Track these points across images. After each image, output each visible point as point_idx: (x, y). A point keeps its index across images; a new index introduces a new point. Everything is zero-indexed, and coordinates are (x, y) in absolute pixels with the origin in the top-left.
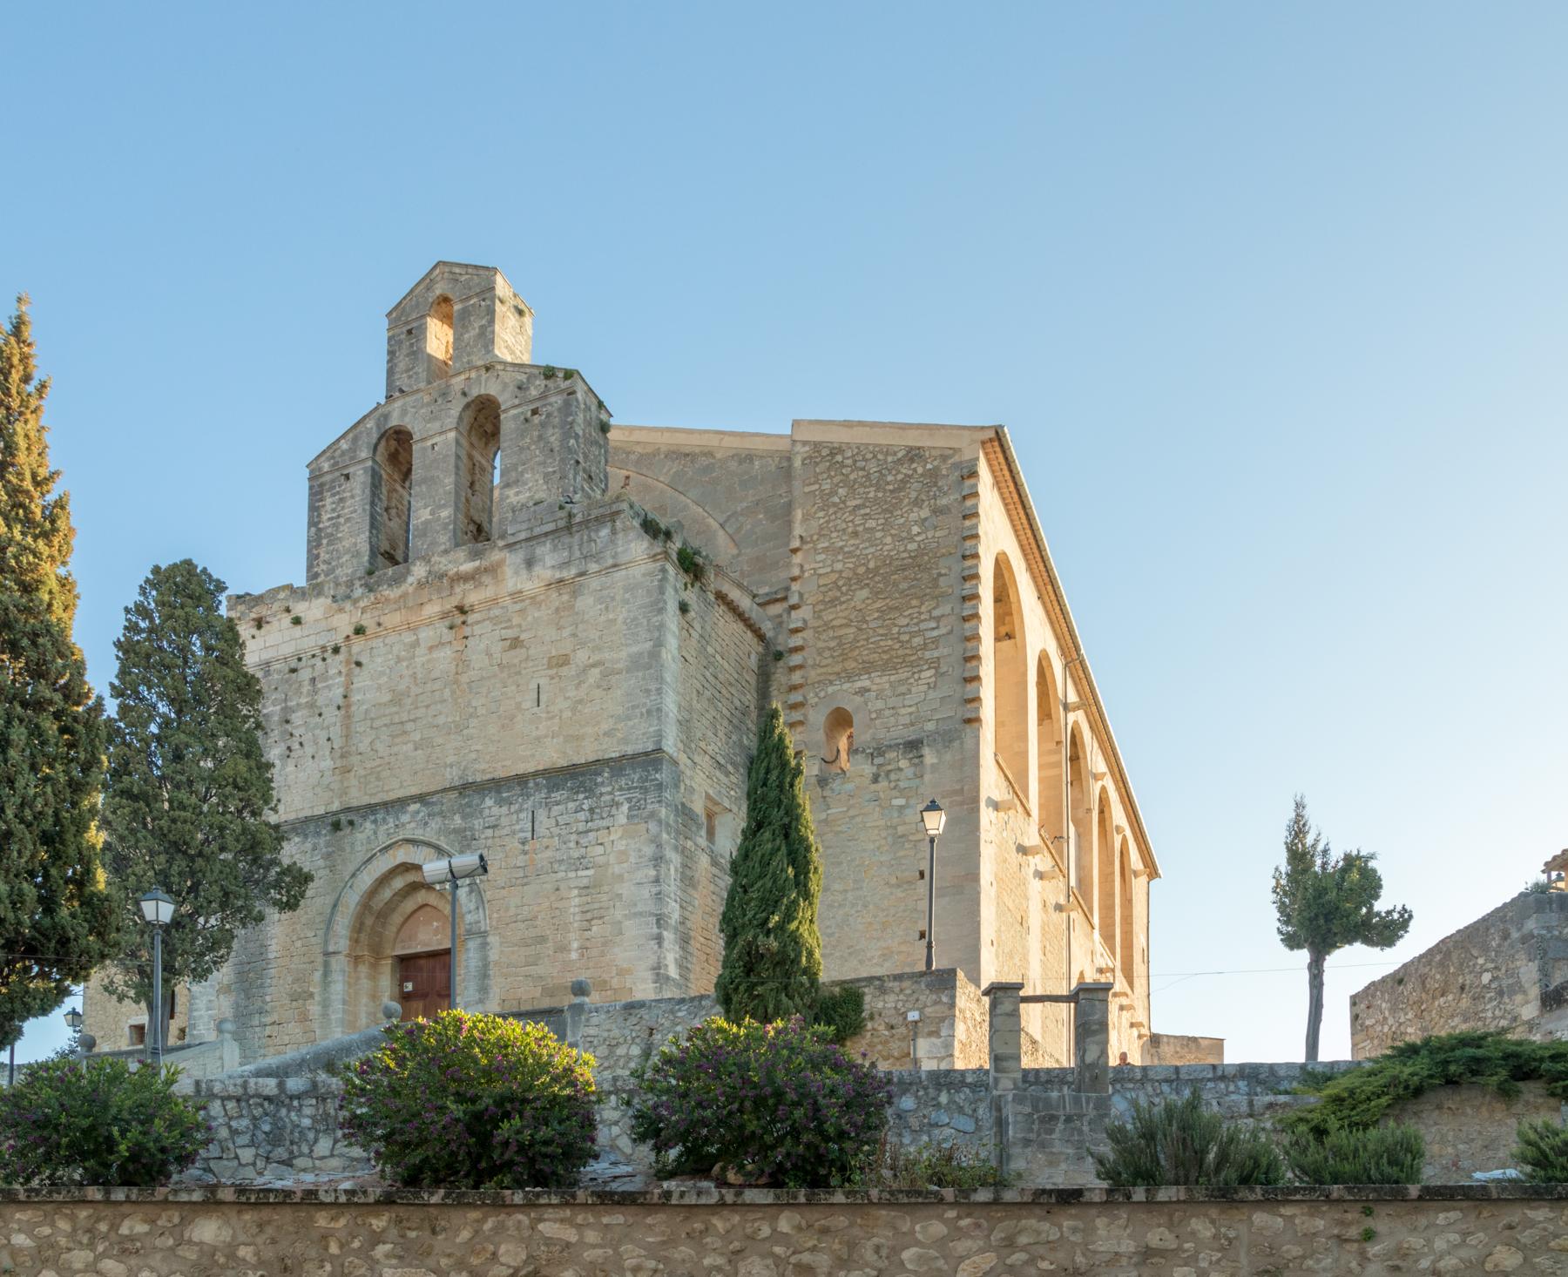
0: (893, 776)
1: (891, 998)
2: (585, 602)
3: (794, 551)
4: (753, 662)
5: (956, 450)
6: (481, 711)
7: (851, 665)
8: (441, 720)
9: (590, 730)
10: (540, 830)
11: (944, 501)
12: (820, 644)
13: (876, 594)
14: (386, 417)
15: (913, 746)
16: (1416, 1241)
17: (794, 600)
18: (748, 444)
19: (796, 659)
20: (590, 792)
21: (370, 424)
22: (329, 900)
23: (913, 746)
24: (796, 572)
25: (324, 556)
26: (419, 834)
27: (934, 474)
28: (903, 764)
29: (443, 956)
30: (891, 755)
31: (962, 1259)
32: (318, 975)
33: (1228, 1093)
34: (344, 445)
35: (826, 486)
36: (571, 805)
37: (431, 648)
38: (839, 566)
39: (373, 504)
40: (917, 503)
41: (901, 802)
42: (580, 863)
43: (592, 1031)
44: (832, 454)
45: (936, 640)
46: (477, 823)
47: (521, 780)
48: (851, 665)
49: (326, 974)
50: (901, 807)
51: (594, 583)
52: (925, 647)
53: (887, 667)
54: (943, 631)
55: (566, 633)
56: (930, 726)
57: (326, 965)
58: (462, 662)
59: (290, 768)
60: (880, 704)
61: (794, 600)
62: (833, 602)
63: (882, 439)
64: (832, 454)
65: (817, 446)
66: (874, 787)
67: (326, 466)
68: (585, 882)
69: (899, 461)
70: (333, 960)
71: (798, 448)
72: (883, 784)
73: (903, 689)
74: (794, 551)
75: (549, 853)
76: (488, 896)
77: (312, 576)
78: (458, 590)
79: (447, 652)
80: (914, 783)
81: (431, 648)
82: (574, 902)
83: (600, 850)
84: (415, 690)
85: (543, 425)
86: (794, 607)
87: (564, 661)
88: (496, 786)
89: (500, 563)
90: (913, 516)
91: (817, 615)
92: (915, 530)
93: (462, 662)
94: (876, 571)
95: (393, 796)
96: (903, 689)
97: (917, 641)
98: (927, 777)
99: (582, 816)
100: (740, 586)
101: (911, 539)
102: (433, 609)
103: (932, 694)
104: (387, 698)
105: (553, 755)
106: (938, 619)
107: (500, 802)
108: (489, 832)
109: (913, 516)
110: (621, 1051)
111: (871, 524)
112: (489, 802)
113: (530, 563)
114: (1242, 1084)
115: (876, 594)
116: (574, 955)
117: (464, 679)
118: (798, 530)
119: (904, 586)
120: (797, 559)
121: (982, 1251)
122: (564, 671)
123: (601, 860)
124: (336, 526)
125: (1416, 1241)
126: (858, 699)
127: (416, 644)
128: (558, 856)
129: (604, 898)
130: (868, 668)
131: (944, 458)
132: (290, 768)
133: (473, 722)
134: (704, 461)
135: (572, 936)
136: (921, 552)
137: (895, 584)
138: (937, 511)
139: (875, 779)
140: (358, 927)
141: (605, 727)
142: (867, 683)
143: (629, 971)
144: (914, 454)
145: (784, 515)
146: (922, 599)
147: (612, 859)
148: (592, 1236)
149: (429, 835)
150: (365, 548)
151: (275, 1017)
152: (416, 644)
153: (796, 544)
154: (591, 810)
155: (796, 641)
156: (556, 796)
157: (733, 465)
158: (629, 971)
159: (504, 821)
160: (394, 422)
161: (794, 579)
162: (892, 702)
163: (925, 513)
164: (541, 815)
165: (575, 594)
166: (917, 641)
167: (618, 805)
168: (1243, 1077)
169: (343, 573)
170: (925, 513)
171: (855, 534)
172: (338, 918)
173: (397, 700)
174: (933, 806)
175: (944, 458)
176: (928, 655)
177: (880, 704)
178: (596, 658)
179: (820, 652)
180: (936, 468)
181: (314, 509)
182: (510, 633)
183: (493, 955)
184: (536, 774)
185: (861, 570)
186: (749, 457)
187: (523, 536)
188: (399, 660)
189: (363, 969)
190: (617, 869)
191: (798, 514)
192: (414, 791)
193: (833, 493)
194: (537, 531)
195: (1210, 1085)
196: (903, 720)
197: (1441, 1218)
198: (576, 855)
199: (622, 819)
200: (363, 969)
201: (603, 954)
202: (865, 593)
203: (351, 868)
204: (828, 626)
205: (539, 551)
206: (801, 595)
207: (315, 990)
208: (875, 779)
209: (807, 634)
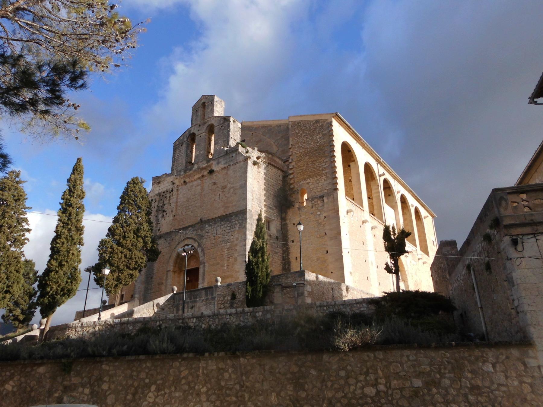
0: (317, 206)
1: (290, 279)
2: (231, 172)
3: (290, 148)
4: (281, 178)
5: (327, 120)
6: (206, 202)
7: (305, 176)
8: (197, 205)
9: (230, 205)
10: (219, 233)
11: (325, 132)
12: (298, 172)
13: (310, 158)
14: (190, 131)
15: (322, 197)
16: (275, 365)
17: (290, 161)
18: (280, 122)
19: (291, 176)
20: (230, 222)
21: (187, 133)
22: (169, 255)
23: (322, 197)
24: (290, 154)
25: (175, 165)
26: (190, 236)
27: (322, 126)
28: (319, 202)
29: (197, 269)
30: (316, 200)
31: (182, 371)
32: (165, 278)
33: (360, 308)
34: (181, 138)
35: (297, 131)
36: (226, 225)
37: (196, 186)
38: (301, 151)
39: (187, 151)
40: (319, 133)
41: (319, 213)
42: (227, 241)
43: (219, 293)
44: (298, 124)
45: (325, 168)
46: (204, 232)
47: (214, 219)
48: (305, 176)
49: (167, 277)
50: (319, 215)
51: (232, 167)
52: (323, 170)
53: (314, 176)
54: (327, 165)
55: (226, 180)
56: (326, 191)
57: (167, 274)
58: (202, 189)
59: (163, 220)
60: (313, 186)
61: (290, 161)
62: (300, 160)
63: (309, 118)
64: (298, 124)
65: (295, 122)
66: (312, 209)
67: (177, 143)
68: (228, 246)
69: (314, 124)
70: (169, 273)
71: (290, 123)
72: (314, 208)
73: (318, 182)
74: (290, 148)
75: (220, 239)
76: (206, 252)
77: (172, 170)
78: (202, 172)
79: (199, 187)
80: (322, 208)
81: (196, 186)
82: (226, 252)
83: (232, 237)
84: (192, 197)
85: (223, 129)
86: (291, 163)
87: (225, 187)
88: (208, 221)
89: (212, 164)
90: (318, 137)
91: (296, 164)
92: (319, 140)
93: (202, 189)
94: (310, 152)
95: (186, 226)
96: (318, 182)
97: (321, 169)
98: (325, 206)
99: (228, 228)
100: (279, 158)
101: (318, 142)
102: (197, 176)
103: (326, 183)
104: (185, 200)
105: (221, 212)
106: (326, 162)
107: (210, 226)
108: (206, 234)
109: (318, 137)
110: (226, 298)
111: (308, 140)
112: (207, 226)
113: (218, 163)
114: (364, 304)
115: (310, 158)
116: (225, 268)
117: (203, 194)
118: (291, 143)
119: (317, 154)
120: (291, 150)
121: (186, 369)
122: (225, 190)
123: (232, 240)
124: (178, 157)
125: (275, 365)
126: (307, 185)
127: (193, 185)
128: (222, 239)
129: (233, 251)
130: (309, 177)
131: (324, 122)
132: (163, 220)
133: (204, 205)
134: (270, 128)
135: (225, 262)
136: (320, 146)
137: (315, 154)
138: (323, 135)
139: (312, 207)
140: (175, 263)
141: (234, 204)
142: (309, 181)
143: (238, 272)
144: (317, 121)
145: (287, 139)
146: (321, 157)
147: (235, 239)
148: (111, 368)
149: (193, 236)
150: (184, 162)
151: (154, 290)
152: (193, 185)
153: (290, 146)
154: (230, 226)
155: (291, 172)
156: (222, 223)
157: (276, 128)
158: (238, 272)
159: (210, 231)
160: (192, 132)
161: (290, 156)
162: (316, 186)
163: (321, 136)
164: (219, 228)
165: (228, 170)
166: (321, 169)
167: (236, 224)
168: (364, 302)
169: (179, 169)
170: (321, 136)
171: (304, 143)
172: (171, 260)
173: (188, 201)
174: (299, 224)
175: (324, 122)
176: (324, 172)
177: (313, 186)
178: (232, 186)
179: (297, 174)
180: (323, 124)
181: (174, 154)
182: (213, 181)
183: (206, 269)
184: (218, 217)
185: (306, 151)
186: (280, 126)
187: (217, 157)
188: (189, 190)
189: (176, 274)
190: (236, 242)
191: (291, 139)
192: (190, 224)
193: (299, 133)
194: (220, 156)
195: (355, 305)
196: (319, 190)
197: (280, 359)
198: (226, 239)
199: (237, 228)
200: (176, 274)
201: (232, 267)
202: (308, 157)
203: (175, 246)
204: (299, 167)
205: (220, 160)
206: (292, 159)
207: (164, 282)
208: (312, 207)
209: (294, 169)
